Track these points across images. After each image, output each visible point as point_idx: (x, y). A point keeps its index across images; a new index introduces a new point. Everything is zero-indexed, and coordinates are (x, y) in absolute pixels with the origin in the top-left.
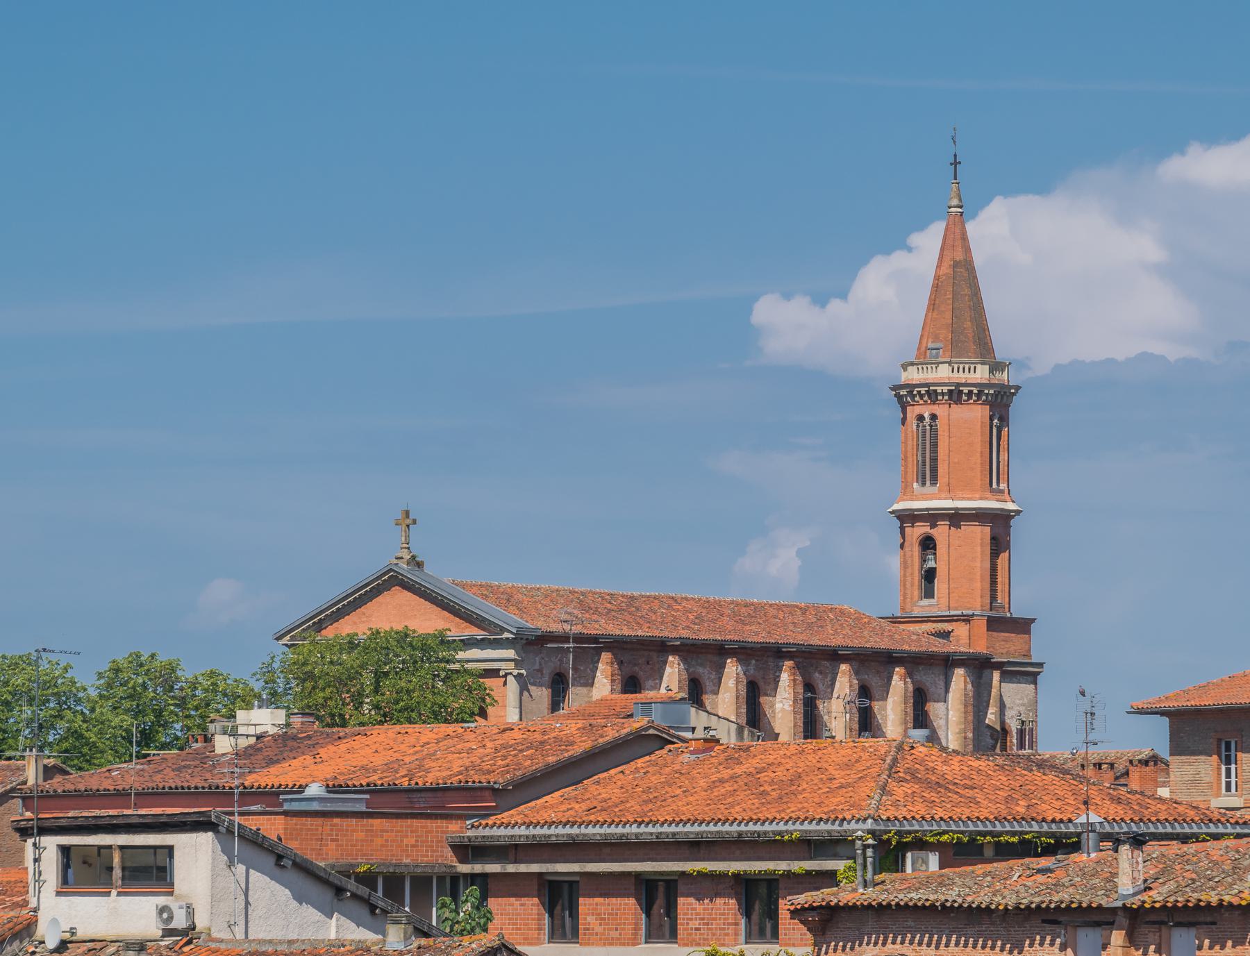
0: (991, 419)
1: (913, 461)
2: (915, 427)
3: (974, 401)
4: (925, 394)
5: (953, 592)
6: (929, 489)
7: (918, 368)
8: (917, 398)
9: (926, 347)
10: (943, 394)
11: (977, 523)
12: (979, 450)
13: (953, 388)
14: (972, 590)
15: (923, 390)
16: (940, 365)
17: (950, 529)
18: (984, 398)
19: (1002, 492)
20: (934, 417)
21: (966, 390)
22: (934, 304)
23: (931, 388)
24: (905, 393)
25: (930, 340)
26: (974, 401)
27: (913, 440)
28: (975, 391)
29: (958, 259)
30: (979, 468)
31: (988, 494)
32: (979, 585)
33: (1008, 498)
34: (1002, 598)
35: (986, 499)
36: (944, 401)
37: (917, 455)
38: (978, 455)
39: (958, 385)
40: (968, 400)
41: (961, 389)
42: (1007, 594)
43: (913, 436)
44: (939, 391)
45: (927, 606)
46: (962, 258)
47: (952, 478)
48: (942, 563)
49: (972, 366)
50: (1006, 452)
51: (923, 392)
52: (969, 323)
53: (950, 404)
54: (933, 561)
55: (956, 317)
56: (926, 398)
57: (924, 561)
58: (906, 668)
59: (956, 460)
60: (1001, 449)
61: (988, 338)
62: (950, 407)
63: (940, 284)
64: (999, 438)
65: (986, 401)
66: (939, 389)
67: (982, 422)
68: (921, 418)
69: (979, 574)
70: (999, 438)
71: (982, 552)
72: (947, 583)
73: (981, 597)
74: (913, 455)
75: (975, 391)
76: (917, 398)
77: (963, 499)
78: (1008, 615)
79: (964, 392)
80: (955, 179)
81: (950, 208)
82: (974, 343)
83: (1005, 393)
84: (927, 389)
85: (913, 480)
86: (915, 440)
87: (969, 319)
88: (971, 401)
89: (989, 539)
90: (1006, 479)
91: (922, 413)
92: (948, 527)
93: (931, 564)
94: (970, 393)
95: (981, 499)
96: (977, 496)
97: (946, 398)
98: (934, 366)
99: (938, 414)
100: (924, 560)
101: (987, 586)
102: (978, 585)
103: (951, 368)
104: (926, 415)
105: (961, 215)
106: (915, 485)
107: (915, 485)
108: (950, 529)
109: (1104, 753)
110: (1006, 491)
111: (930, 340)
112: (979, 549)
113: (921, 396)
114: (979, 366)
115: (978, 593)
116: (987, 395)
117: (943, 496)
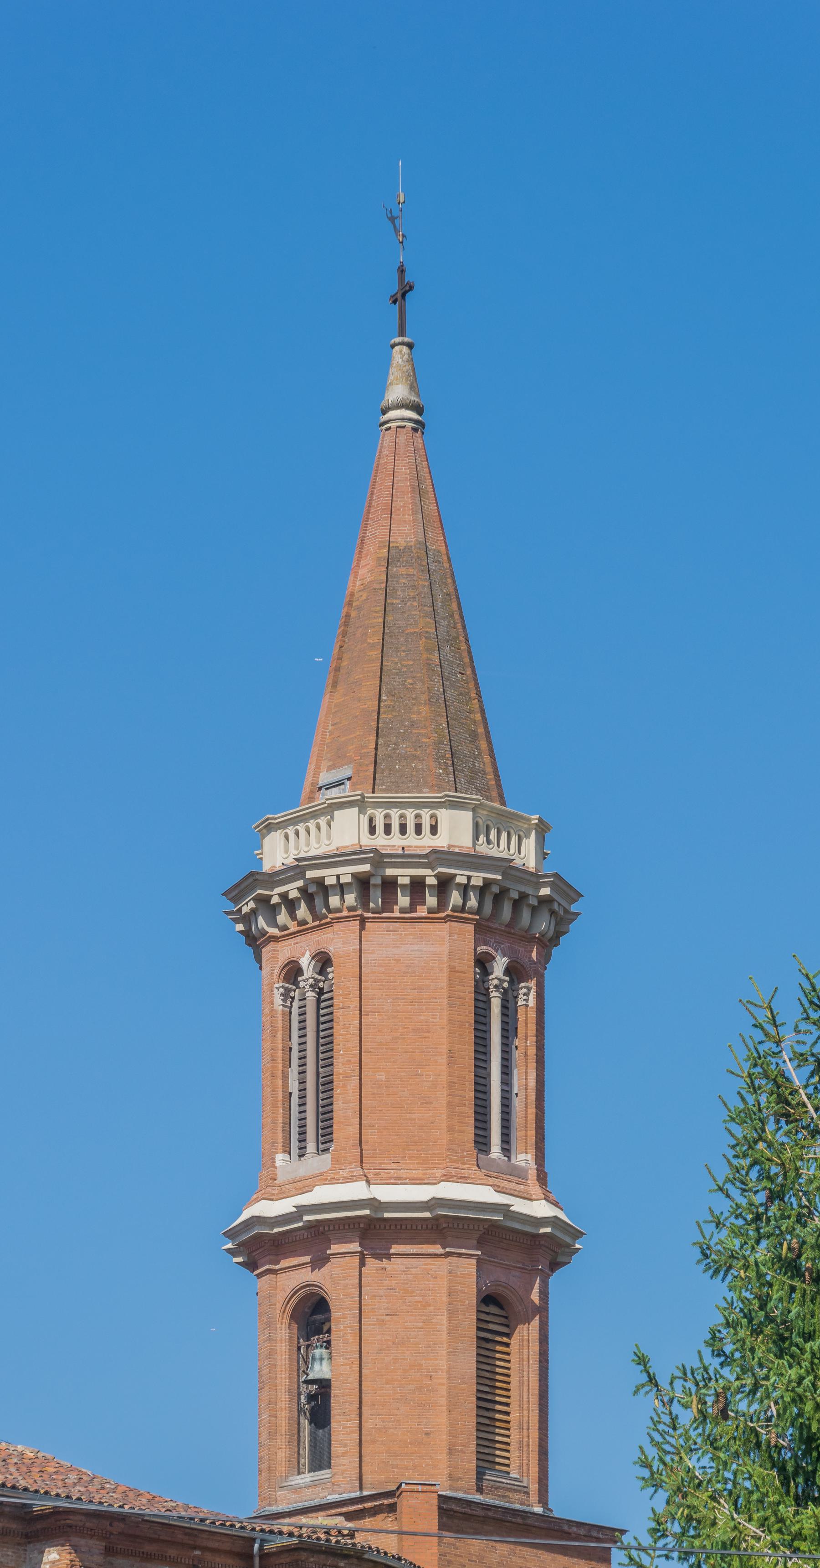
0: (483, 963)
1: (274, 1091)
2: (278, 1000)
3: (430, 911)
4: (297, 899)
5: (374, 1442)
6: (315, 1163)
7: (287, 837)
8: (283, 917)
9: (313, 784)
10: (342, 888)
11: (438, 1249)
12: (444, 1049)
13: (366, 868)
14: (427, 1434)
15: (292, 889)
16: (337, 814)
17: (362, 1264)
18: (455, 898)
19: (519, 1174)
20: (324, 961)
21: (404, 874)
22: (337, 669)
23: (310, 874)
24: (252, 905)
25: (325, 764)
26: (430, 911)
27: (273, 1035)
28: (431, 881)
29: (400, 541)
30: (442, 1096)
31: (471, 1170)
32: (442, 1420)
33: (535, 1189)
34: (521, 1466)
35: (463, 1179)
36: (345, 913)
37: (285, 1078)
38: (443, 1060)
39: (379, 859)
40: (412, 908)
41: (389, 872)
42: (534, 1456)
43: (273, 1025)
44: (330, 881)
45: (308, 1487)
46: (412, 539)
47: (372, 1126)
48: (342, 1360)
49: (426, 814)
50: (532, 1065)
51: (293, 894)
52: (425, 710)
53: (363, 921)
54: (325, 1363)
55: (390, 694)
56: (302, 911)
57: (304, 1361)
58: (76, 1549)
59: (381, 1076)
60: (517, 1055)
61: (487, 758)
62: (362, 927)
63: (353, 614)
64: (509, 1031)
65: (463, 909)
66: (329, 876)
67: (452, 970)
68: (293, 972)
69: (443, 1390)
70: (509, 1031)
71: (453, 1329)
72: (355, 1415)
73: (450, 1452)
74: (273, 1076)
75: (431, 881)
76: (283, 917)
77: (398, 1181)
78: (538, 1510)
79: (400, 881)
80: (402, 333)
81: (384, 412)
82: (437, 760)
83: (523, 896)
84: (300, 883)
85: (274, 1147)
86: (279, 1035)
87: (423, 698)
88: (422, 911)
89: (474, 1301)
90: (532, 1139)
91: (294, 955)
92: (357, 1260)
93: (320, 1370)
94: (417, 887)
95: (447, 1178)
96: (439, 1173)
97: (351, 899)
98: (322, 821)
99: (331, 950)
100: (304, 1361)
101: (470, 1421)
102: (441, 1421)
103: (365, 820)
104: (305, 962)
105: (419, 427)
106: (280, 1159)
107: (280, 1159)
108: (362, 1264)
109: (212, 1513)
110: (532, 1173)
111: (325, 764)
112: (443, 1320)
113: (291, 905)
114: (443, 815)
115: (442, 1439)
116: (465, 889)
117: (344, 1173)
